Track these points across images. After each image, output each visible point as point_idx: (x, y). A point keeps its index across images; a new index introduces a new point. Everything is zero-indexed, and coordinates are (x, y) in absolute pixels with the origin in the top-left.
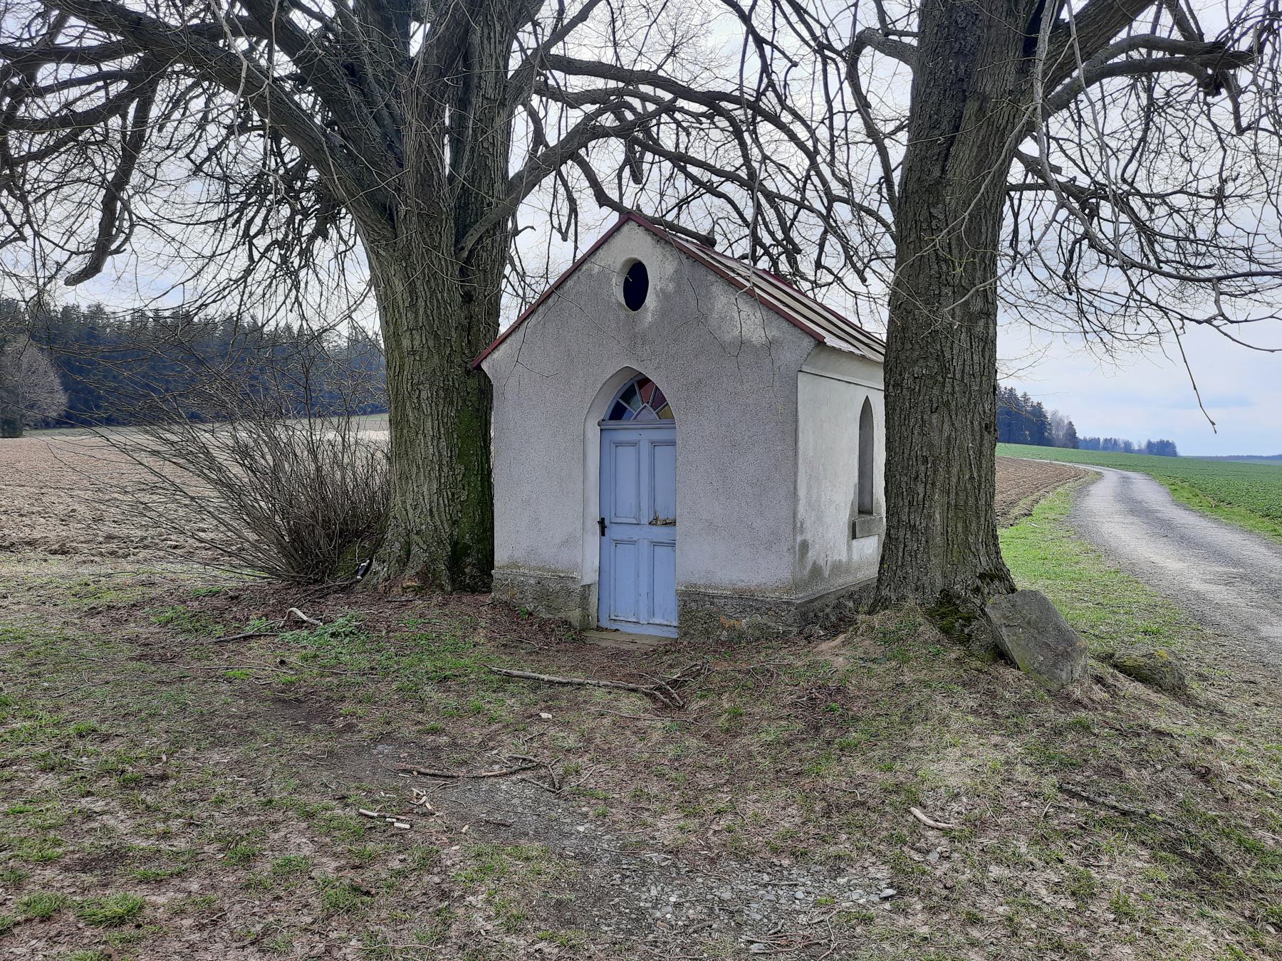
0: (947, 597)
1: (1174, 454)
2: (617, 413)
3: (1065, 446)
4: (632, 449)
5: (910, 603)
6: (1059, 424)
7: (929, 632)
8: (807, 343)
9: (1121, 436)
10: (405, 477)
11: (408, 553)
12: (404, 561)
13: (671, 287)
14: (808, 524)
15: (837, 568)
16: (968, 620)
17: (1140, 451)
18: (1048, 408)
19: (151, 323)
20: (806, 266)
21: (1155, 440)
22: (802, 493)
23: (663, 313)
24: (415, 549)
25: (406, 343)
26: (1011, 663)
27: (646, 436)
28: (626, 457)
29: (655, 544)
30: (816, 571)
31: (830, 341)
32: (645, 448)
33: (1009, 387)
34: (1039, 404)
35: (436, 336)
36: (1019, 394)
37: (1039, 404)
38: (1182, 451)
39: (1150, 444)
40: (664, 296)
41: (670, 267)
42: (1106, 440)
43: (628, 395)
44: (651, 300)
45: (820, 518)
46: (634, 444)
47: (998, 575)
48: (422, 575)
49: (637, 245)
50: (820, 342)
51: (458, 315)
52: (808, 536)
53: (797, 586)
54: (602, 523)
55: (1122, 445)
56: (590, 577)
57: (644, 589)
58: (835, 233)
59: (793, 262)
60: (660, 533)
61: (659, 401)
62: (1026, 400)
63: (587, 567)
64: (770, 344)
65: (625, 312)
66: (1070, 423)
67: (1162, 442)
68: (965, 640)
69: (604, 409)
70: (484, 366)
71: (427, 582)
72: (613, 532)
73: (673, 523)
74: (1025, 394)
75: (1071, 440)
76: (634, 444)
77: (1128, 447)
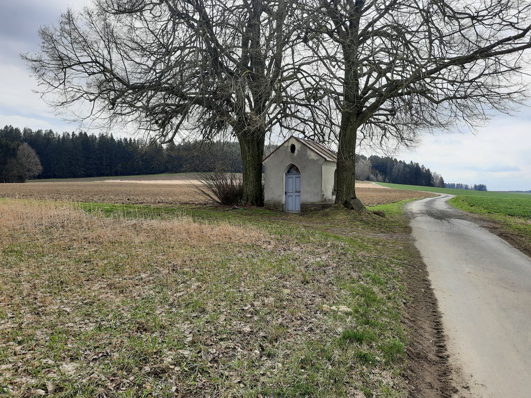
0: (346, 202)
1: (486, 190)
2: (289, 172)
3: (439, 187)
4: (292, 179)
5: (340, 202)
6: (437, 178)
7: (342, 206)
8: (324, 160)
9: (464, 183)
10: (247, 184)
11: (248, 199)
12: (247, 200)
13: (300, 149)
14: (324, 191)
15: (329, 200)
16: (349, 205)
17: (472, 189)
18: (432, 171)
19: (71, 137)
20: (326, 138)
21: (478, 184)
22: (323, 186)
23: (298, 154)
24: (249, 198)
25: (247, 158)
26: (353, 209)
27: (294, 176)
28: (290, 180)
29: (296, 196)
30: (325, 200)
31: (328, 159)
32: (294, 178)
33: (416, 163)
34: (428, 169)
35: (253, 157)
36: (420, 166)
37: (428, 169)
38: (489, 189)
39: (476, 186)
40: (298, 151)
41: (300, 146)
42: (457, 184)
43: (291, 168)
44: (296, 151)
45: (326, 190)
46: (292, 177)
47: (355, 198)
48: (251, 203)
49: (293, 142)
50: (326, 159)
51: (257, 153)
52: (324, 193)
53: (322, 201)
54: (286, 192)
55: (464, 187)
56: (284, 203)
57: (294, 204)
58: (332, 131)
59: (323, 138)
60: (297, 194)
61: (297, 169)
62: (423, 168)
63: (283, 199)
64: (318, 159)
65: (291, 154)
66: (441, 177)
67: (480, 185)
68: (348, 207)
69: (286, 172)
70: (263, 163)
71: (253, 204)
72: (289, 194)
73: (300, 192)
74: (423, 166)
75: (442, 184)
76: (292, 177)
77: (466, 187)
